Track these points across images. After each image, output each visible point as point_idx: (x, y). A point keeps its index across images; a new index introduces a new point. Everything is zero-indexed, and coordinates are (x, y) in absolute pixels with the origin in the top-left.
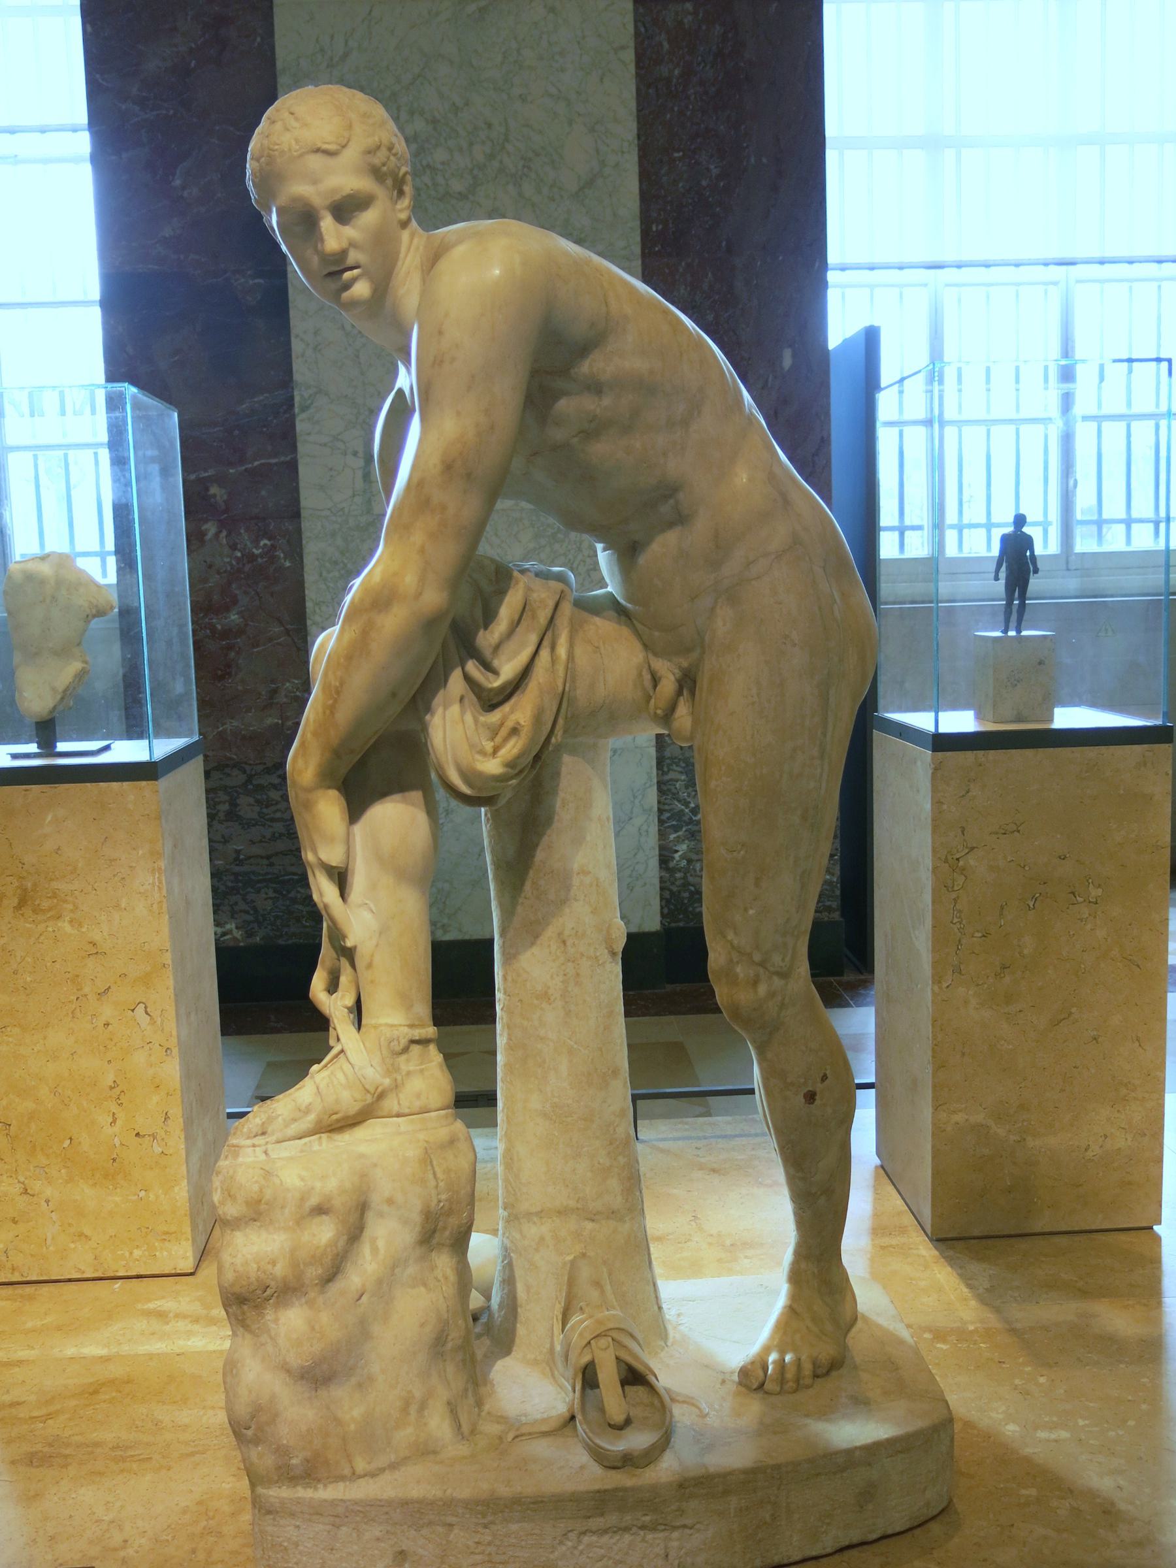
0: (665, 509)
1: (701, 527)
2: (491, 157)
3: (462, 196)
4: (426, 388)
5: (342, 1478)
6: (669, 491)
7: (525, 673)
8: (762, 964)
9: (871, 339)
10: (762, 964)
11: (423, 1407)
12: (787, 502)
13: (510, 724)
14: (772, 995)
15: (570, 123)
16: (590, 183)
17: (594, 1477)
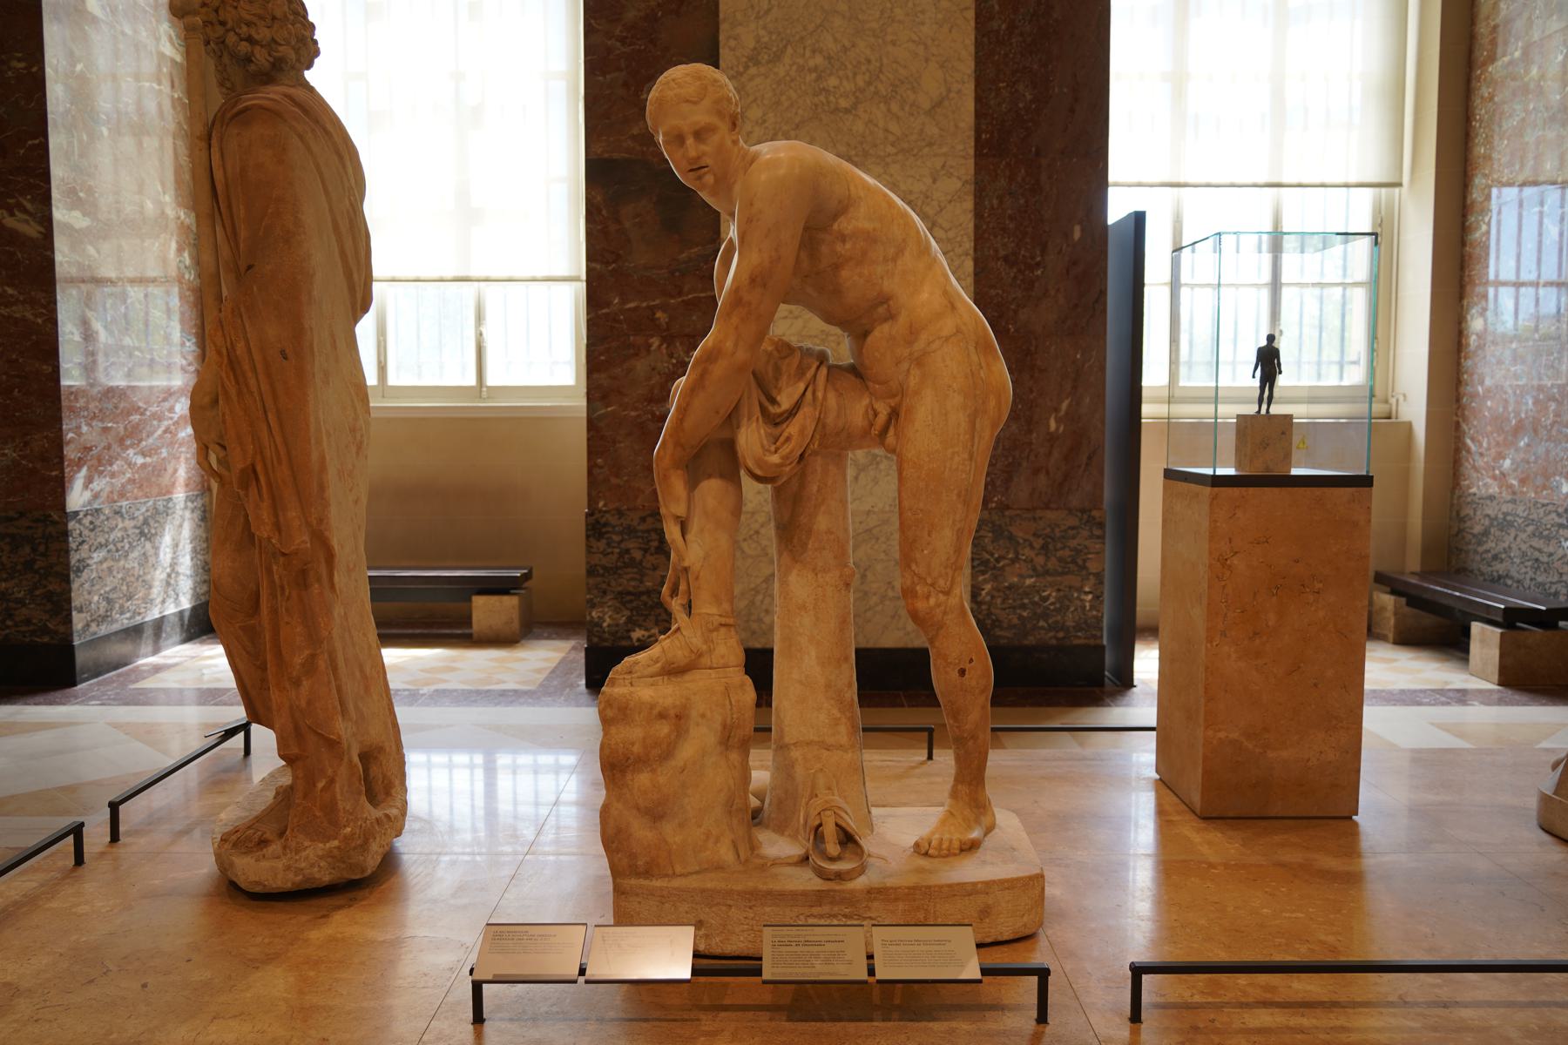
0: (881, 310)
1: (903, 319)
2: (869, 83)
3: (847, 111)
4: (743, 237)
5: (666, 875)
6: (884, 299)
7: (797, 407)
8: (932, 585)
9: (1139, 219)
10: (932, 585)
11: (717, 841)
12: (953, 308)
13: (785, 434)
14: (938, 605)
15: (927, 60)
16: (939, 104)
17: (817, 884)
